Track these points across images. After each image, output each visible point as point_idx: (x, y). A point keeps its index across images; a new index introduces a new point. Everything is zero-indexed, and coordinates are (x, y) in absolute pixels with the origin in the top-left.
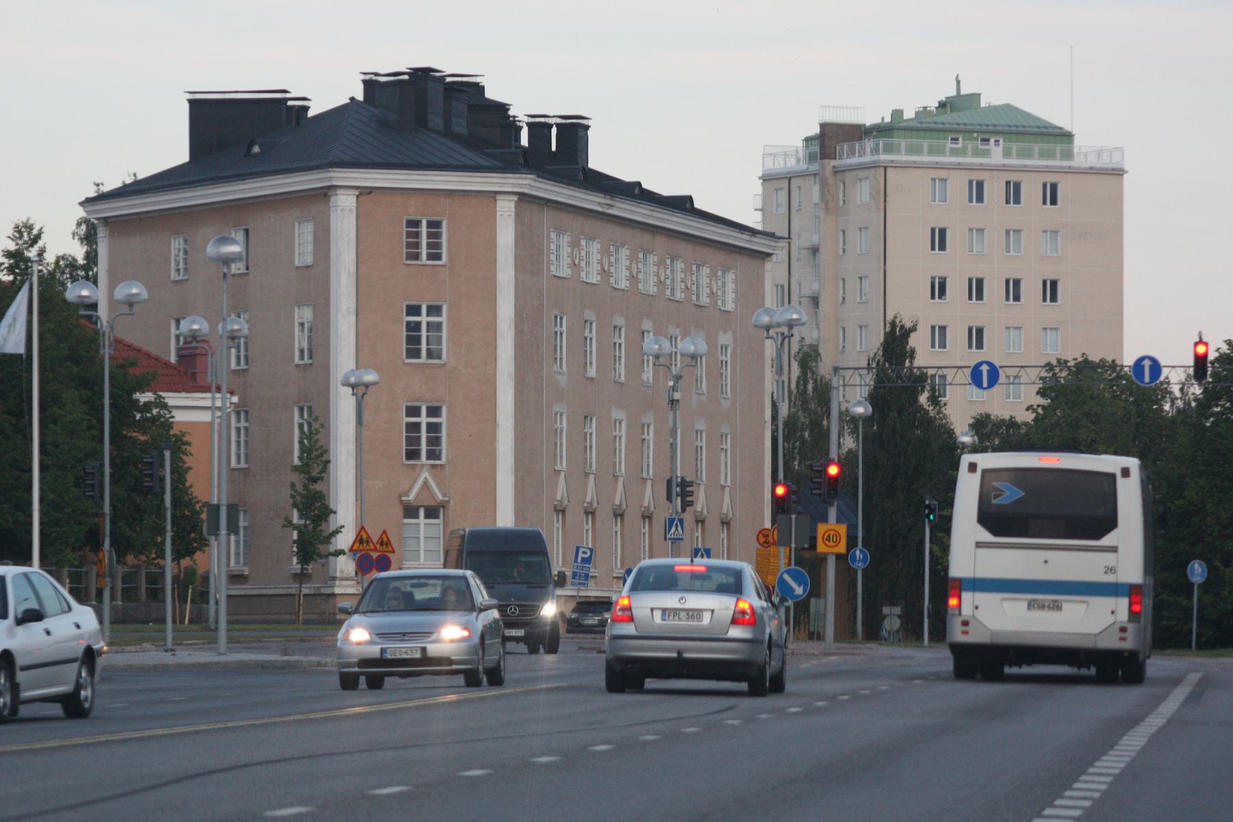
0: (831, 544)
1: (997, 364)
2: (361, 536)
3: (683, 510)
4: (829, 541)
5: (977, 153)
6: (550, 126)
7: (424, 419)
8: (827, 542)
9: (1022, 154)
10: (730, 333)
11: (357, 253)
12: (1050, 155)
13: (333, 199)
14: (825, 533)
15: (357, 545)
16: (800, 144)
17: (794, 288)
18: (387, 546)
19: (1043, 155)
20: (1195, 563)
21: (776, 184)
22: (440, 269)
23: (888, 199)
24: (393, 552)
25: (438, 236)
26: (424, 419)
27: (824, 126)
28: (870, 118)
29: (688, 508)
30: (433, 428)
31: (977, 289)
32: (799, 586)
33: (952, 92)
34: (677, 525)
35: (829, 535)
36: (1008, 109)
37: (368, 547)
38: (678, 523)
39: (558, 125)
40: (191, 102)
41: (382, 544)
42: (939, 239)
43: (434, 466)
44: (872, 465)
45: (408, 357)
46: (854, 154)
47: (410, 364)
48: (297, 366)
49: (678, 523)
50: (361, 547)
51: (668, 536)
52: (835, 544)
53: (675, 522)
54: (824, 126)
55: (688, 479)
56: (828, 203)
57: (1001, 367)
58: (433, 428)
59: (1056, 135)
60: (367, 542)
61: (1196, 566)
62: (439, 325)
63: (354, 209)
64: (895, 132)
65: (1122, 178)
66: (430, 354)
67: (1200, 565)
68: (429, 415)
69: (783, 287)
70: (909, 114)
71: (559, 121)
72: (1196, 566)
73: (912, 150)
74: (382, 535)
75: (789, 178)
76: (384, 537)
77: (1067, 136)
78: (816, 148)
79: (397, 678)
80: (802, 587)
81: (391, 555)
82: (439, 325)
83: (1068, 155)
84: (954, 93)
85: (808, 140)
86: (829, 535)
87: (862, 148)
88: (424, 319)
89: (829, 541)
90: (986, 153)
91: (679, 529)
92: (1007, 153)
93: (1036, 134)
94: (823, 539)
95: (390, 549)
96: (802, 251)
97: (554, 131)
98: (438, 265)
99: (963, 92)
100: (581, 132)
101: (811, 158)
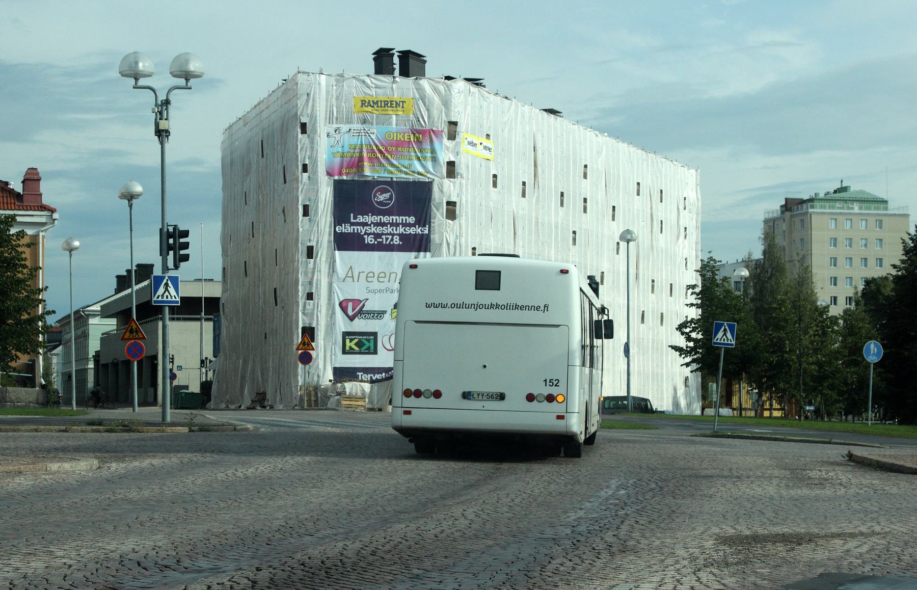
2: (132, 327)
3: (176, 267)
5: (849, 208)
9: (867, 209)
12: (878, 209)
15: (128, 334)
16: (779, 208)
18: (137, 333)
19: (875, 209)
20: (871, 343)
24: (313, 349)
29: (183, 264)
34: (167, 284)
36: (862, 192)
37: (137, 336)
38: (169, 282)
42: (834, 262)
44: (366, 182)
46: (798, 210)
49: (169, 282)
50: (131, 336)
53: (165, 281)
54: (786, 199)
59: (880, 201)
60: (137, 332)
61: (872, 346)
64: (816, 203)
65: (908, 218)
67: (876, 345)
72: (872, 346)
73: (821, 207)
75: (774, 220)
77: (886, 202)
78: (784, 208)
81: (311, 352)
83: (886, 209)
84: (840, 187)
85: (782, 206)
87: (802, 208)
90: (852, 208)
92: (861, 208)
93: (872, 201)
101: (782, 212)
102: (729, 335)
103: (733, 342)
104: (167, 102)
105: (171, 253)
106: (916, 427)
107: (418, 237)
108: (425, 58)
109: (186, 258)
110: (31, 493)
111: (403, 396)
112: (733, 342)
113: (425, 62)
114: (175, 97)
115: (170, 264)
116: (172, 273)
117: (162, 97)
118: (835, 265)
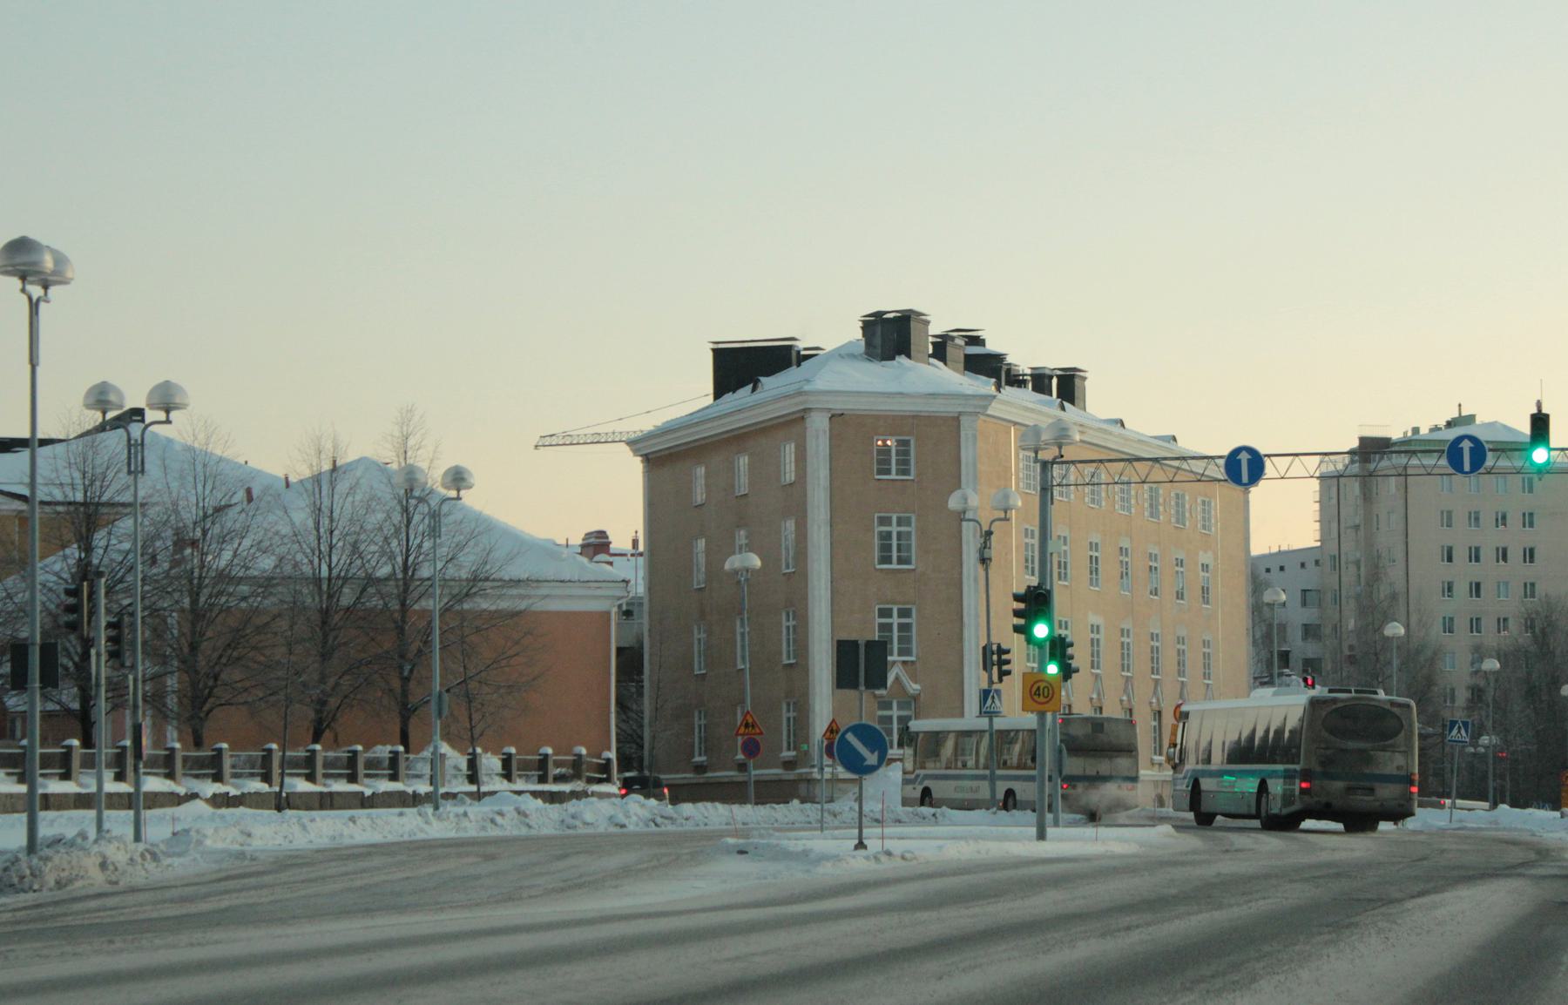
0: (1042, 699)
1: (1262, 451)
3: (1001, 680)
4: (1039, 695)
6: (1051, 377)
7: (895, 620)
8: (1036, 697)
10: (1210, 554)
11: (830, 469)
13: (808, 421)
14: (1032, 686)
17: (1343, 557)
21: (1329, 481)
22: (909, 483)
23: (1409, 490)
25: (907, 453)
26: (895, 620)
27: (1363, 440)
28: (1396, 434)
29: (1005, 678)
30: (904, 628)
31: (1475, 555)
32: (872, 752)
33: (1456, 415)
34: (993, 697)
35: (1039, 688)
39: (1058, 376)
40: (714, 350)
41: (747, 726)
42: (1448, 519)
43: (904, 663)
45: (880, 563)
47: (882, 570)
48: (784, 574)
51: (984, 710)
52: (1045, 700)
54: (1363, 440)
55: (1004, 646)
56: (1367, 496)
57: (1266, 456)
58: (904, 628)
60: (753, 726)
62: (909, 533)
63: (827, 429)
66: (900, 561)
68: (900, 616)
69: (1335, 557)
70: (1424, 431)
71: (1059, 373)
74: (746, 716)
75: (1339, 476)
76: (834, 725)
79: (896, 841)
80: (876, 753)
82: (909, 533)
86: (1039, 688)
88: (894, 529)
89: (1039, 695)
91: (996, 701)
94: (1031, 692)
95: (758, 731)
96: (1349, 530)
97: (1055, 381)
98: (907, 480)
99: (1463, 414)
100: (1077, 381)
102: (1463, 732)
103: (1467, 740)
104: (989, 533)
105: (995, 669)
106: (6, 471)
107: (634, 447)
108: (928, 318)
109: (1008, 673)
110: (8, 864)
111: (825, 756)
112: (1467, 740)
113: (928, 322)
114: (995, 527)
115: (995, 677)
116: (995, 687)
117: (985, 528)
118: (1449, 525)
